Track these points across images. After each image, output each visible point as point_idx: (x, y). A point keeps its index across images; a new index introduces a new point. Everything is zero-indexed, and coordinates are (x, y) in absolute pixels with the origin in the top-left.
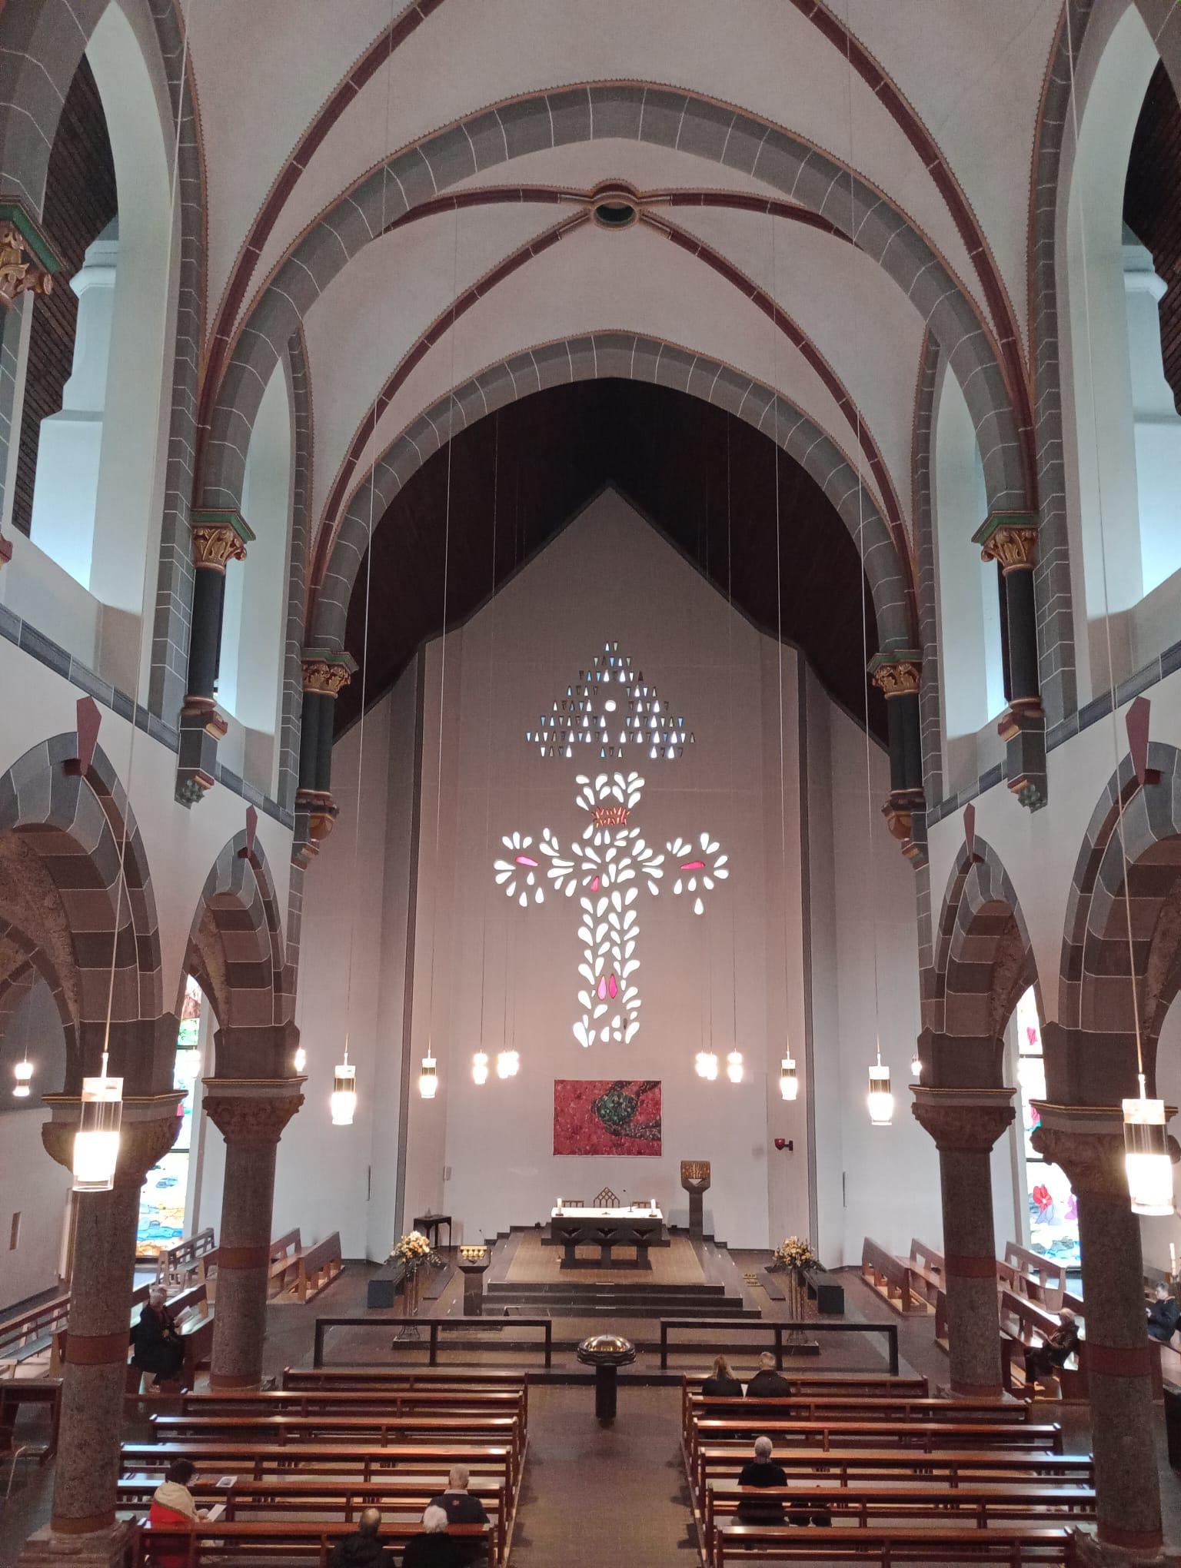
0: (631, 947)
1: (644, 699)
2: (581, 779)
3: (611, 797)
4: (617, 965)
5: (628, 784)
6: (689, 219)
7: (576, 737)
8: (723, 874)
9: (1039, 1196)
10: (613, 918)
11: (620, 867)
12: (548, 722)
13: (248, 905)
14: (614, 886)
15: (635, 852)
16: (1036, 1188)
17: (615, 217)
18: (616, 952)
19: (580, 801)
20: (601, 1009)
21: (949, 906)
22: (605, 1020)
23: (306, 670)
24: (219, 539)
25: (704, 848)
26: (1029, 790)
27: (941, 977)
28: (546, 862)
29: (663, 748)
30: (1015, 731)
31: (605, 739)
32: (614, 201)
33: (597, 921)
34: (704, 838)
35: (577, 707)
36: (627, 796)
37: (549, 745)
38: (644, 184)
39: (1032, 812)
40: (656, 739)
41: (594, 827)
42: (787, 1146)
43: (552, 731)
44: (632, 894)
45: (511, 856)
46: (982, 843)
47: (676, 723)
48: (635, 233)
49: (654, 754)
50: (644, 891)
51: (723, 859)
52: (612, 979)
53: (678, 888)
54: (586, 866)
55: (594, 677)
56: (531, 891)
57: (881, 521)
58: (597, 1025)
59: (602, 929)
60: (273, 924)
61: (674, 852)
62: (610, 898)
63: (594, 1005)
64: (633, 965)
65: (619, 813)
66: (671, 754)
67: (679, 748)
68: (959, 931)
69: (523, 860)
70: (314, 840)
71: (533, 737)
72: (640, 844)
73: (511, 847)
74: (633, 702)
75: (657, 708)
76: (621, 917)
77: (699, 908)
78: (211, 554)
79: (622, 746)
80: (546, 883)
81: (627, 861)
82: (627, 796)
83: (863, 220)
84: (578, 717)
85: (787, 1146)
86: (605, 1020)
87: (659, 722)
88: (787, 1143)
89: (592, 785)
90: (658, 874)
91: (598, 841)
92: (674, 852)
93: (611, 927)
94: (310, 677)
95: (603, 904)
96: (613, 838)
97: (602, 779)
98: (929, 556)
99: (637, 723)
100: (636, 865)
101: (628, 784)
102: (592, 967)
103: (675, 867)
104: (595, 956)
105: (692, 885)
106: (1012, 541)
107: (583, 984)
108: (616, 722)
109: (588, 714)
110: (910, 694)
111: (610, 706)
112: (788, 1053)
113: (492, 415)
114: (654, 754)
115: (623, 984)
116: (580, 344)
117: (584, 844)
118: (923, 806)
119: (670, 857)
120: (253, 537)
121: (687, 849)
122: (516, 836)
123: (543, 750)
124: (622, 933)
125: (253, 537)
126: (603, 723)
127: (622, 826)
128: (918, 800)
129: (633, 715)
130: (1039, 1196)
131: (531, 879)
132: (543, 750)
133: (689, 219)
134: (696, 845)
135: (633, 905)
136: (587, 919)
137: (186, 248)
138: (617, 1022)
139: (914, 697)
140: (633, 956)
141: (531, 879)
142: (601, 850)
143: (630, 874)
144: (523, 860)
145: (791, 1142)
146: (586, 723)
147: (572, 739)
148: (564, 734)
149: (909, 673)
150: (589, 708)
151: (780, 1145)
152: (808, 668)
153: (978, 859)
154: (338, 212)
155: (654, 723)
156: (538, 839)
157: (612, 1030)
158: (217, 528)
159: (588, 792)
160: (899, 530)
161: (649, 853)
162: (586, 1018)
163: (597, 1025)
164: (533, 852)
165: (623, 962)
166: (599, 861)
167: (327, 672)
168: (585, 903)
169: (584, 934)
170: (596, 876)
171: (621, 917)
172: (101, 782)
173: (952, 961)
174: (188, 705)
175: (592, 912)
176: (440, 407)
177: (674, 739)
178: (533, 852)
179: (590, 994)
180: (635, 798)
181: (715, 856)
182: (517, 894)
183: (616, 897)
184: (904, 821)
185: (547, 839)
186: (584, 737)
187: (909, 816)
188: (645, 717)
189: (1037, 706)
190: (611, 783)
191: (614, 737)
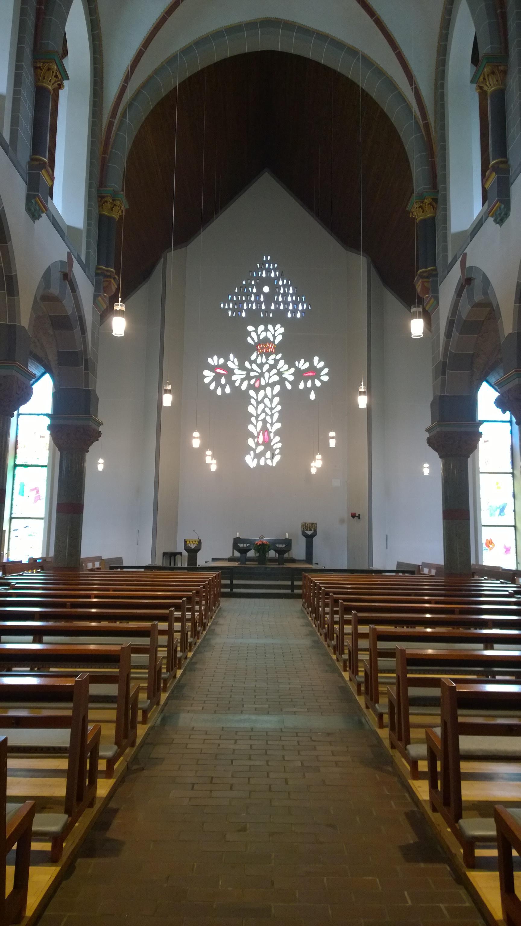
0: (276, 416)
1: (284, 286)
2: (250, 328)
3: (266, 338)
4: (268, 426)
5: (275, 331)
7: (248, 306)
8: (325, 378)
9: (488, 544)
10: (267, 401)
11: (271, 375)
12: (232, 298)
13: (69, 313)
14: (267, 385)
15: (278, 367)
16: (487, 540)
18: (268, 419)
19: (249, 340)
20: (260, 448)
21: (450, 320)
22: (262, 454)
23: (100, 201)
24: (49, 69)
25: (315, 365)
26: (500, 209)
27: (444, 364)
28: (231, 372)
29: (294, 311)
31: (263, 307)
33: (258, 403)
34: (316, 359)
35: (248, 290)
36: (274, 337)
37: (233, 310)
39: (501, 226)
40: (291, 307)
41: (257, 353)
42: (357, 517)
43: (234, 303)
44: (277, 388)
45: (212, 368)
47: (301, 299)
49: (289, 315)
50: (283, 387)
51: (326, 370)
52: (265, 429)
53: (301, 386)
54: (252, 374)
55: (257, 274)
56: (223, 387)
57: (417, 122)
58: (258, 456)
59: (261, 406)
60: (83, 330)
61: (299, 367)
62: (265, 390)
63: (257, 447)
64: (278, 425)
65: (270, 346)
66: (299, 315)
67: (302, 311)
68: (455, 333)
69: (218, 371)
70: (106, 294)
71: (224, 306)
72: (282, 362)
73: (213, 364)
74: (279, 287)
75: (291, 291)
76: (271, 401)
77: (313, 396)
78: (44, 78)
79: (272, 311)
80: (231, 383)
81: (274, 371)
82: (274, 337)
84: (250, 294)
85: (357, 517)
86: (262, 454)
87: (292, 299)
88: (357, 515)
89: (256, 331)
90: (291, 378)
91: (259, 361)
92: (299, 367)
93: (266, 406)
94: (102, 206)
95: (262, 393)
96: (267, 359)
97: (261, 328)
98: (443, 138)
99: (280, 299)
100: (279, 373)
101: (275, 331)
102: (256, 426)
103: (299, 375)
104: (257, 421)
105: (309, 384)
106: (493, 73)
107: (251, 435)
108: (269, 298)
109: (254, 294)
110: (430, 217)
111: (266, 289)
112: (362, 383)
113: (202, 71)
114: (289, 315)
115: (272, 435)
116: (251, 25)
117: (251, 362)
118: (437, 275)
119: (298, 370)
120: (68, 78)
121: (307, 365)
122: (215, 357)
123: (230, 313)
124: (271, 409)
125: (68, 78)
126: (262, 299)
127: (272, 353)
128: (434, 273)
129: (278, 294)
130: (488, 544)
131: (223, 381)
132: (230, 313)
134: (312, 364)
135: (278, 395)
136: (252, 401)
138: (268, 455)
139: (433, 219)
140: (278, 421)
141: (223, 381)
142: (261, 366)
143: (276, 378)
144: (218, 371)
145: (359, 515)
146: (253, 299)
147: (245, 307)
148: (242, 302)
149: (430, 204)
150: (255, 291)
151: (353, 516)
152: (372, 269)
155: (289, 299)
156: (227, 359)
157: (266, 459)
158: (47, 63)
159: (254, 335)
160: (427, 126)
161: (286, 367)
162: (252, 452)
163: (258, 456)
164: (224, 367)
165: (272, 424)
166: (260, 371)
167: (111, 203)
168: (252, 393)
169: (251, 409)
170: (258, 378)
171: (271, 401)
172: (74, 288)
173: (451, 352)
174: (32, 160)
175: (256, 398)
176: (172, 60)
177: (300, 307)
178: (224, 367)
179: (254, 440)
180: (279, 339)
181: (322, 369)
182: (216, 388)
183: (268, 389)
184: (426, 284)
185: (232, 360)
186: (252, 306)
187: (429, 282)
188: (285, 295)
189: (506, 162)
190: (266, 330)
191: (268, 306)
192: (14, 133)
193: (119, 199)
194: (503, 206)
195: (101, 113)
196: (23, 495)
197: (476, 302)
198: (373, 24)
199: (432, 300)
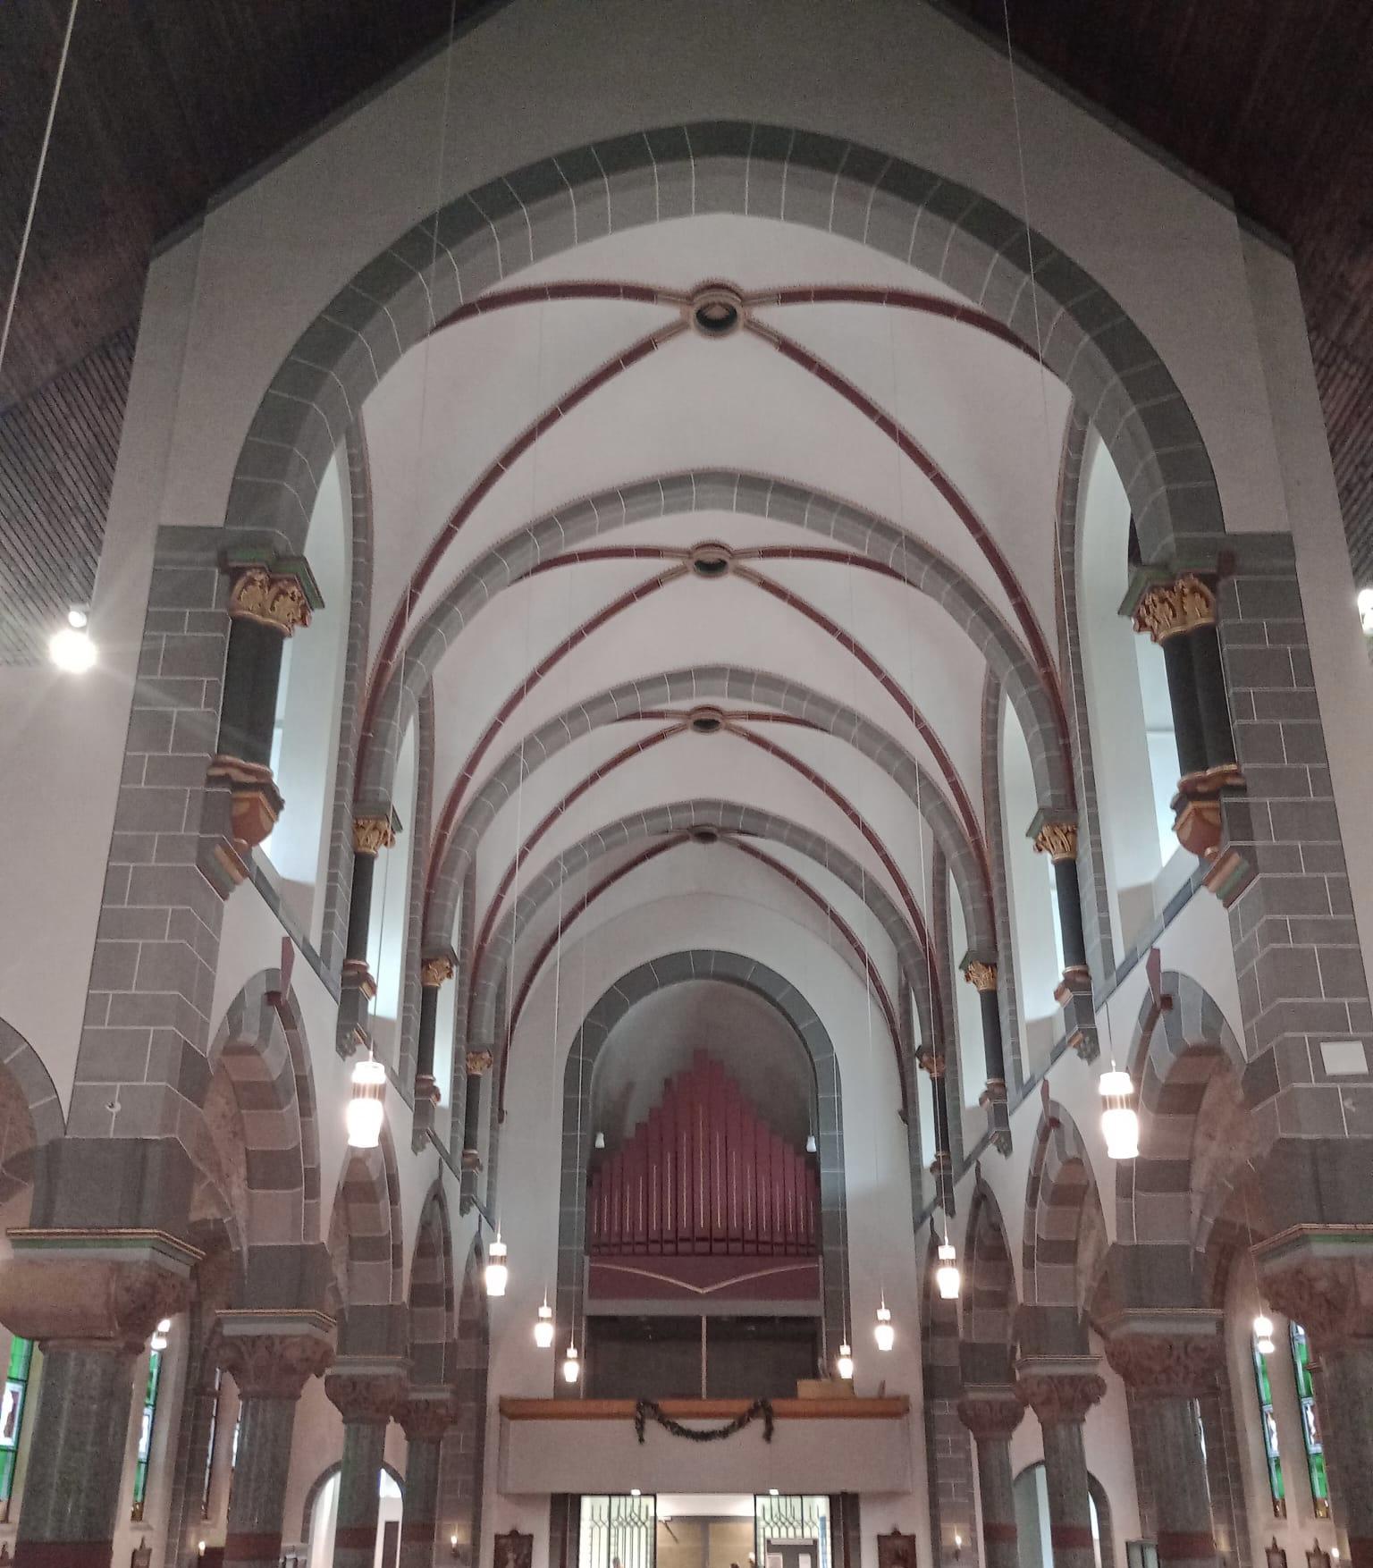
6: (771, 568)
13: (375, 1177)
17: (711, 569)
24: (375, 828)
30: (1068, 995)
32: (711, 556)
38: (735, 544)
39: (1089, 1064)
46: (1056, 1105)
48: (727, 583)
60: (394, 1199)
83: (924, 573)
133: (768, 568)
137: (355, 593)
153: (1055, 1123)
154: (485, 566)
172: (290, 1018)
192: (326, 940)
193: (291, 576)
194: (1087, 1039)
195: (430, 810)
196: (1127, 1543)
197: (1189, 1043)
198: (931, 484)
199: (1235, 859)
